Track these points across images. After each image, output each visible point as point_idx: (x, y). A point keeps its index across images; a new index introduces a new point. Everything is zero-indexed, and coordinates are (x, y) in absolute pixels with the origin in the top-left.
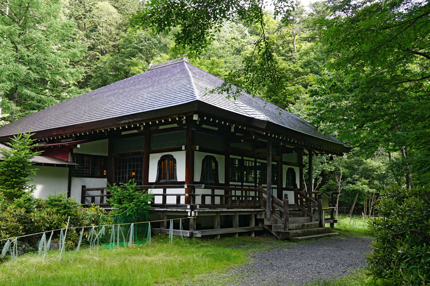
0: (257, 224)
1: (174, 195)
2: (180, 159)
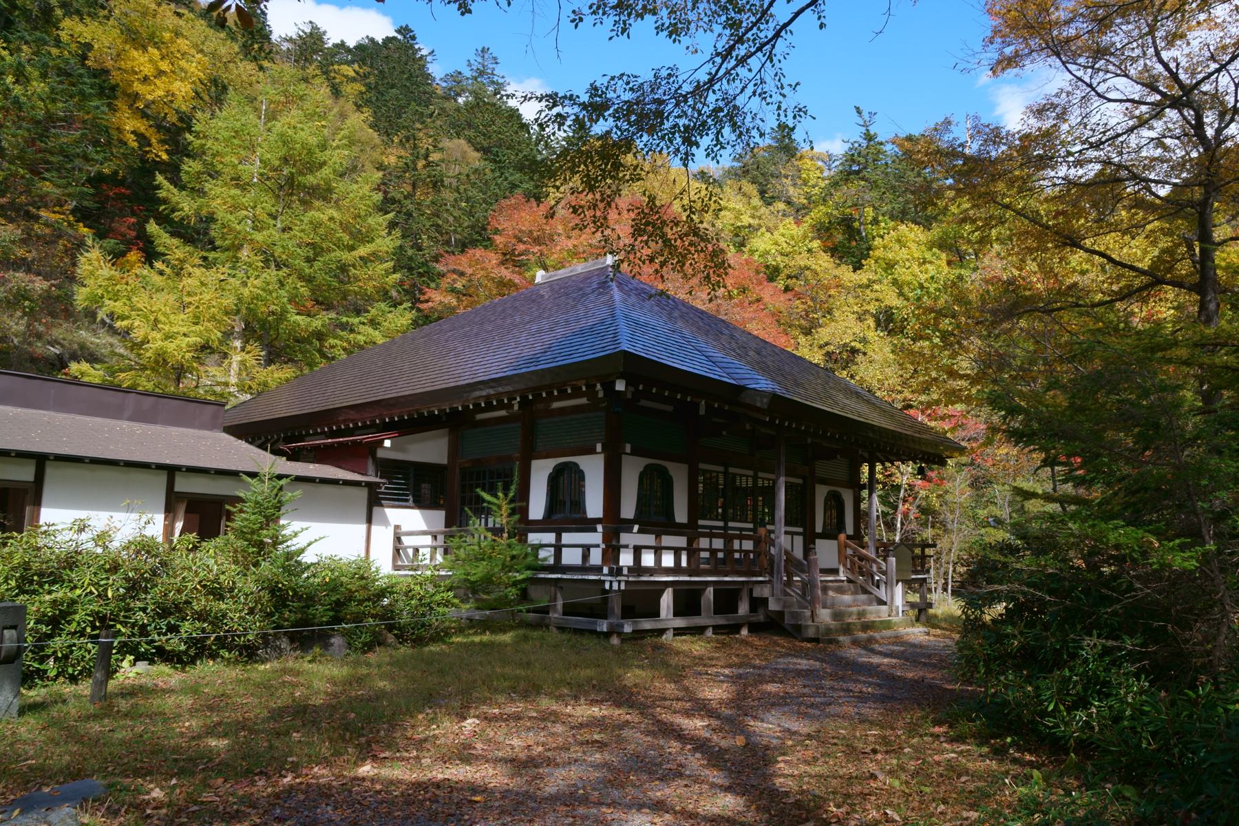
1: (579, 548)
2: (593, 469)
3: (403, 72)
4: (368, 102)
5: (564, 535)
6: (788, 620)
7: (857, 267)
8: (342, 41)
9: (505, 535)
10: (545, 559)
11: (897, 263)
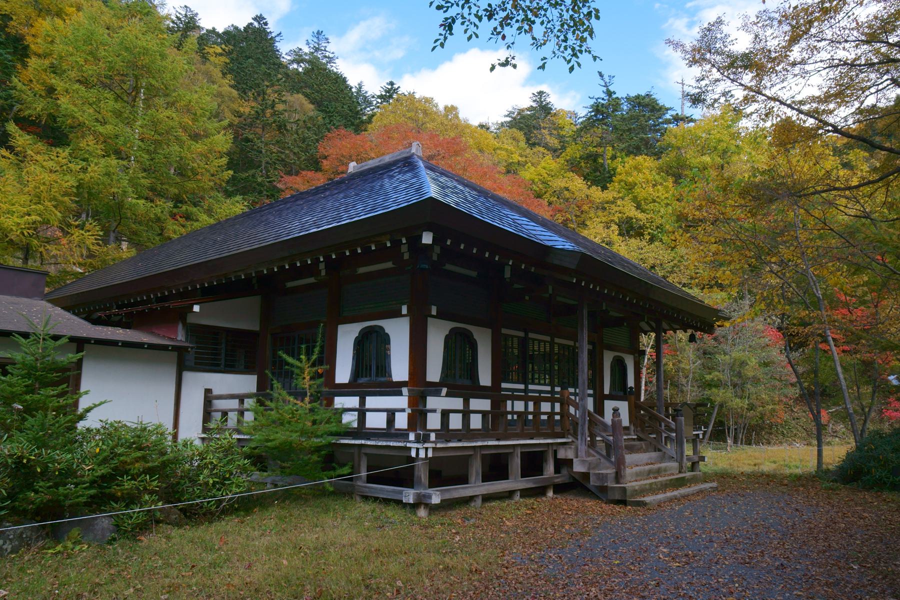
0: (557, 470)
1: (383, 410)
2: (398, 333)
3: (257, 48)
4: (231, 71)
5: (368, 399)
6: (593, 482)
7: (604, 188)
8: (214, 28)
9: (307, 399)
10: (350, 423)
11: (636, 184)
